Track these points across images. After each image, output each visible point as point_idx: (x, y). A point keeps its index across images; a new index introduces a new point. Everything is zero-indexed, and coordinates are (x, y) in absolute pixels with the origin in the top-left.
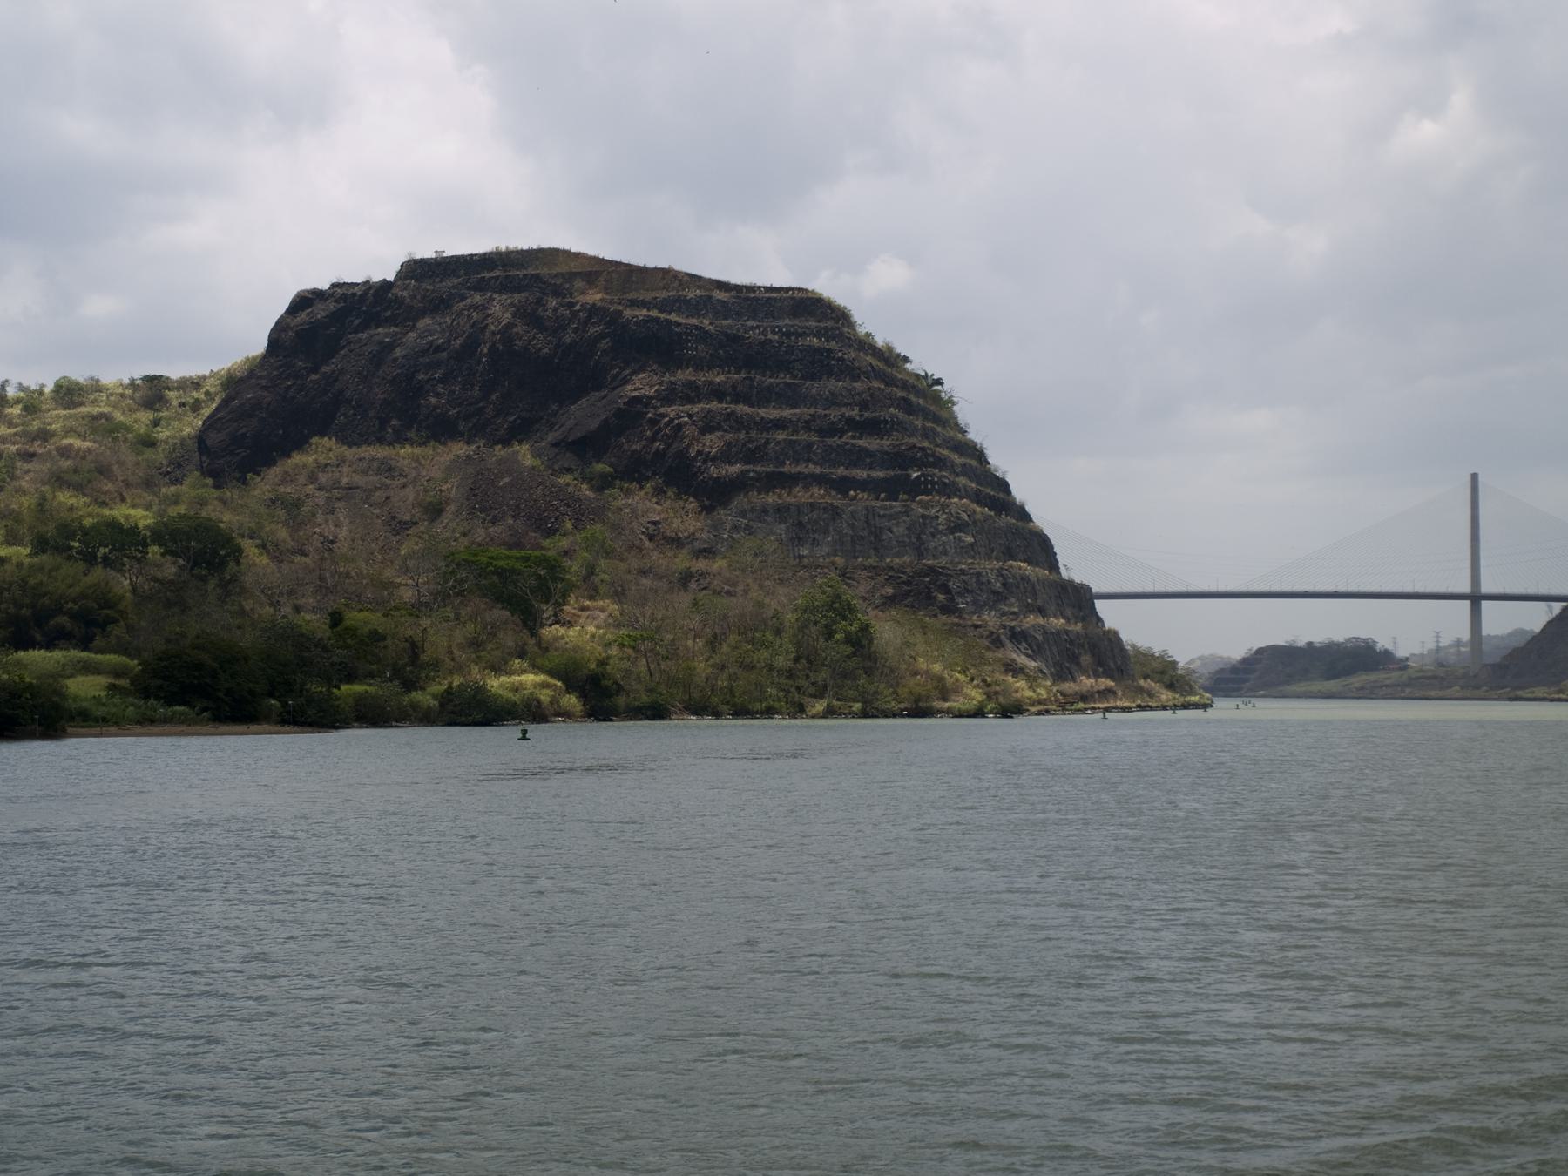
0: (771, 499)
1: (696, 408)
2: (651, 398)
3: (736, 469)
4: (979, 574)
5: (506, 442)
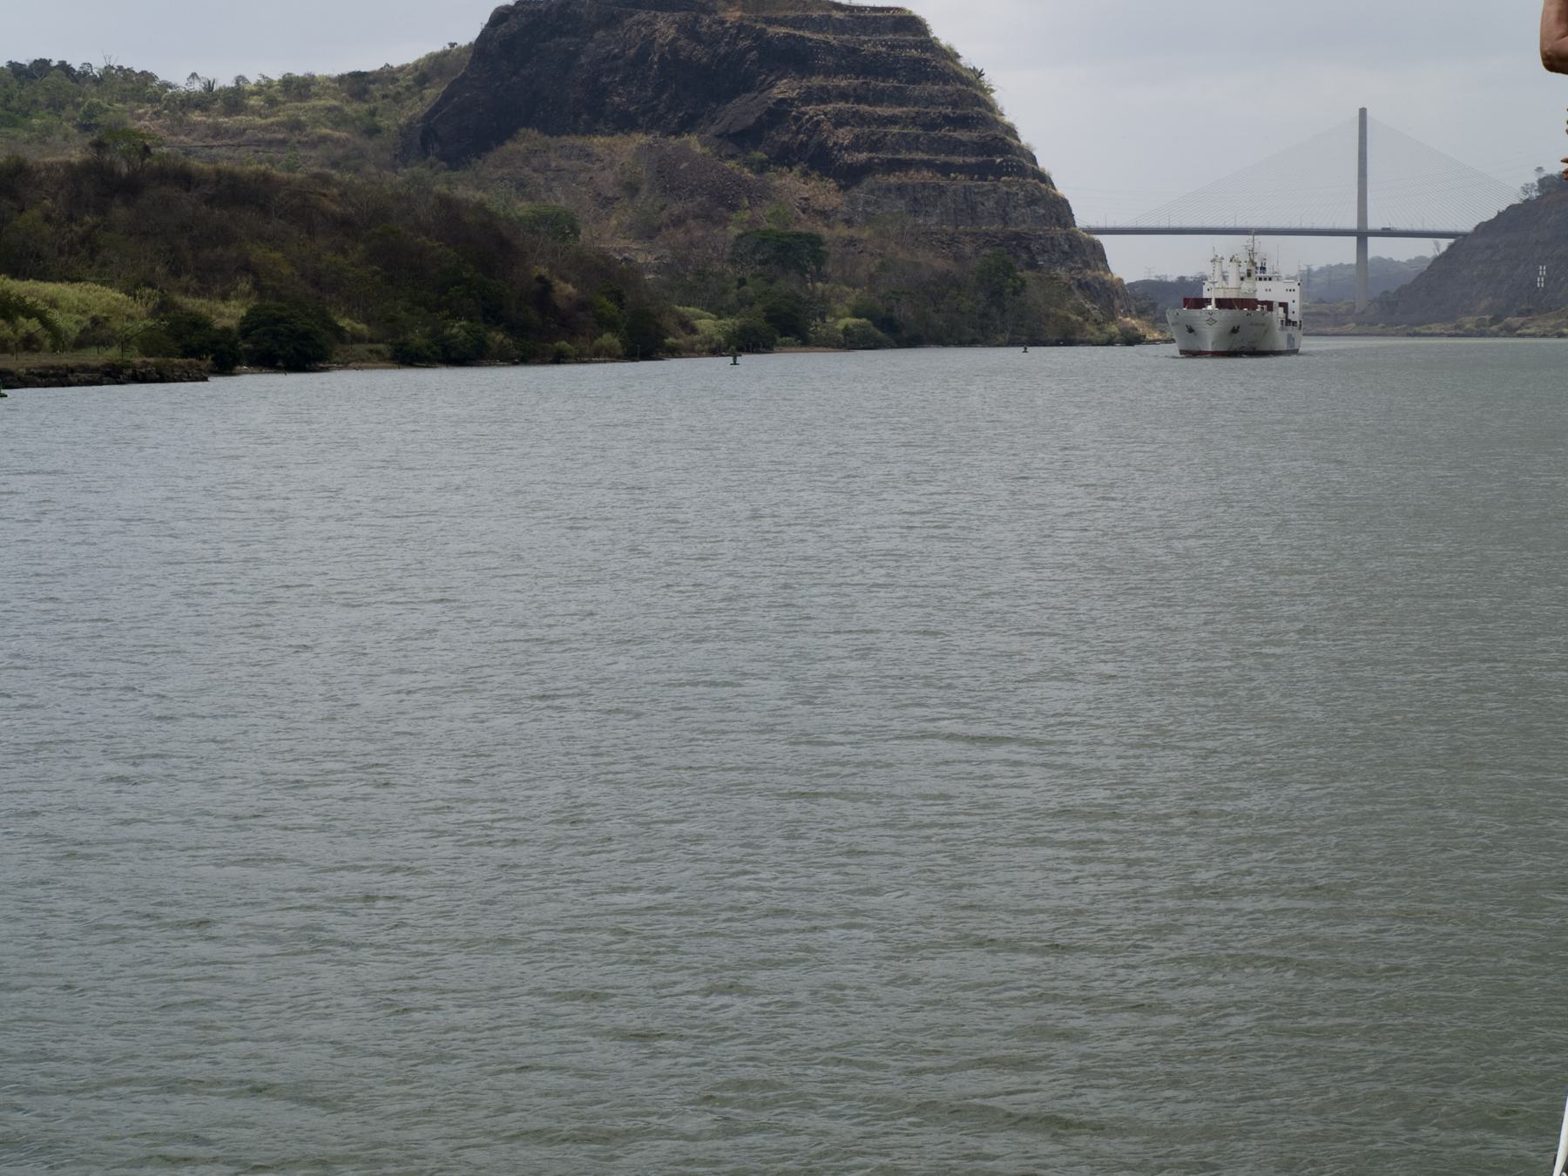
0: (892, 180)
1: (829, 107)
2: (793, 99)
3: (864, 156)
4: (1052, 238)
5: (678, 134)
